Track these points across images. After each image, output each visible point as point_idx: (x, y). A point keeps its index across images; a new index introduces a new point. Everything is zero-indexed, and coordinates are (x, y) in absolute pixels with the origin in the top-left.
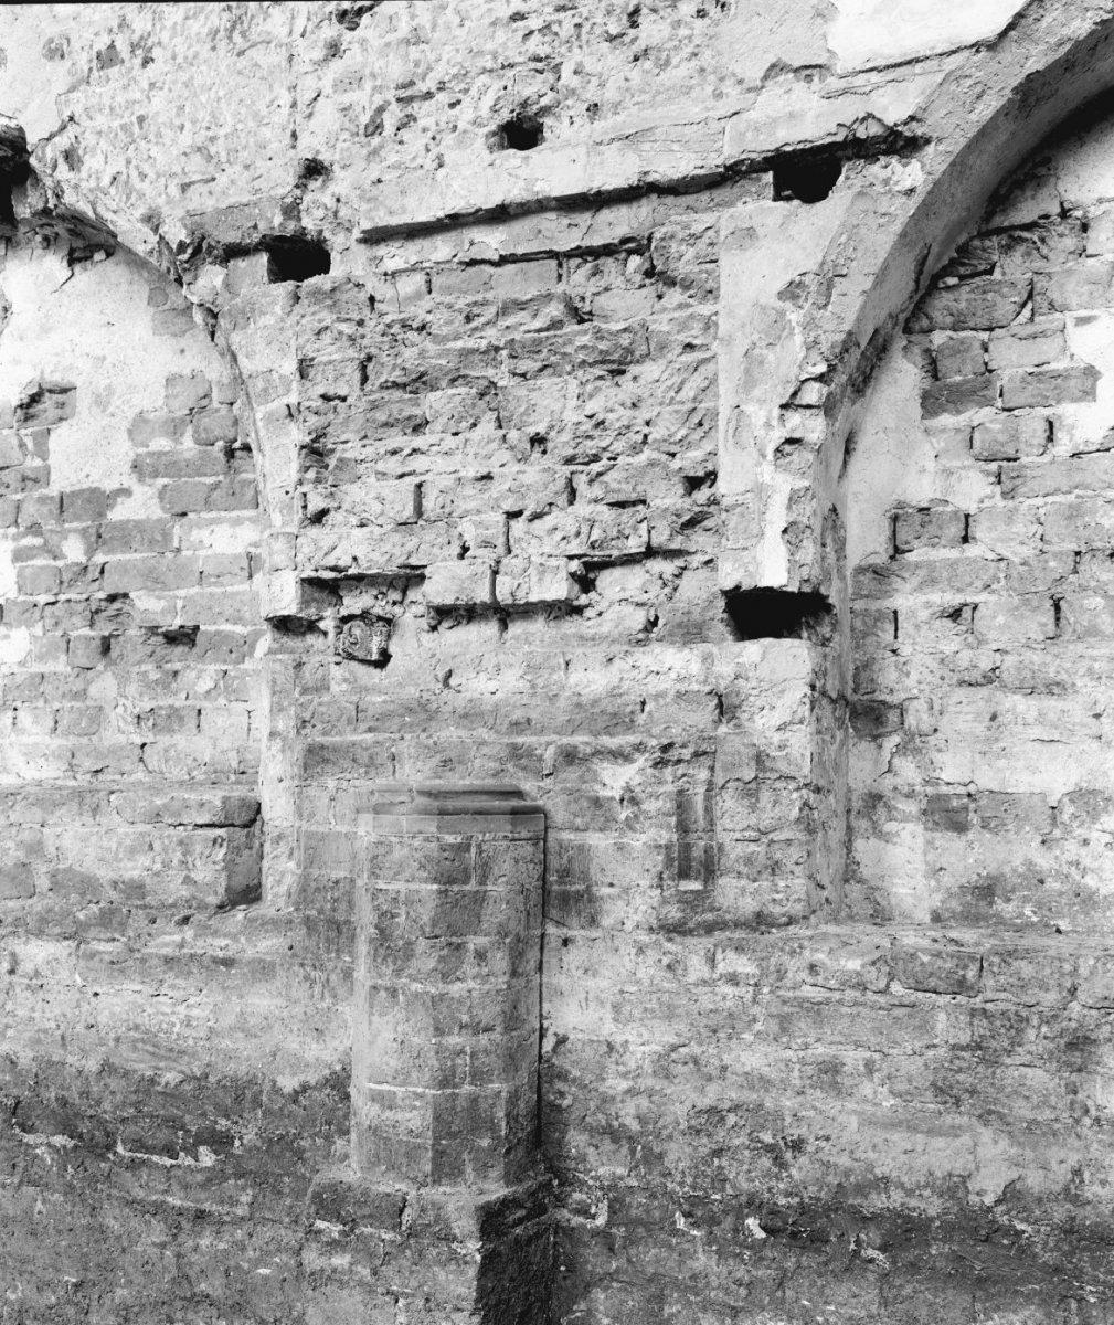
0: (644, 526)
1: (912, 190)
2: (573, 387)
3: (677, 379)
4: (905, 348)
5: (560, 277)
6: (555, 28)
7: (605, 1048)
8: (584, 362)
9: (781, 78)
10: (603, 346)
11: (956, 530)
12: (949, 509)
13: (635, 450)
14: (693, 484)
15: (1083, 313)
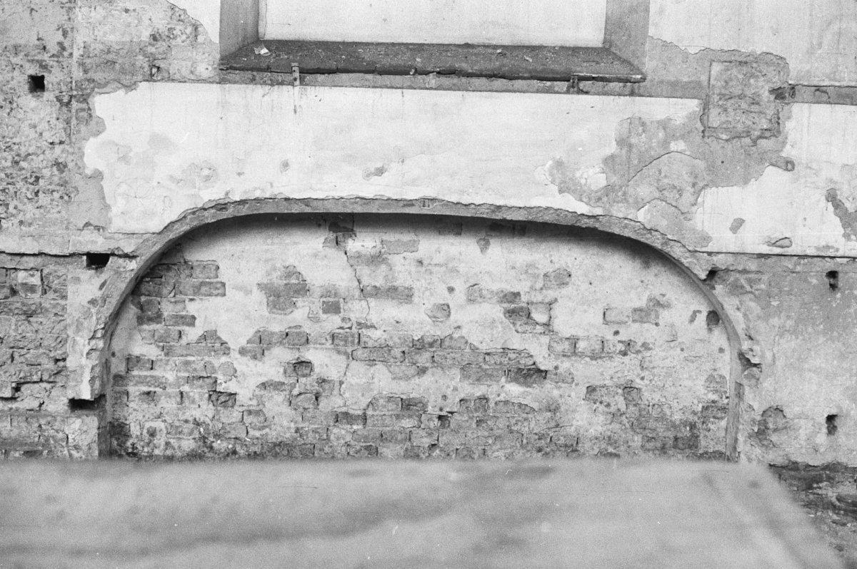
0: (40, 372)
1: (132, 270)
2: (14, 320)
3: (52, 325)
4: (132, 300)
5: (7, 275)
6: (7, 191)
7: (304, 340)
8: (17, 314)
9: (89, 227)
10: (25, 308)
11: (148, 366)
12: (146, 358)
13: (36, 348)
14: (57, 361)
15: (191, 297)
